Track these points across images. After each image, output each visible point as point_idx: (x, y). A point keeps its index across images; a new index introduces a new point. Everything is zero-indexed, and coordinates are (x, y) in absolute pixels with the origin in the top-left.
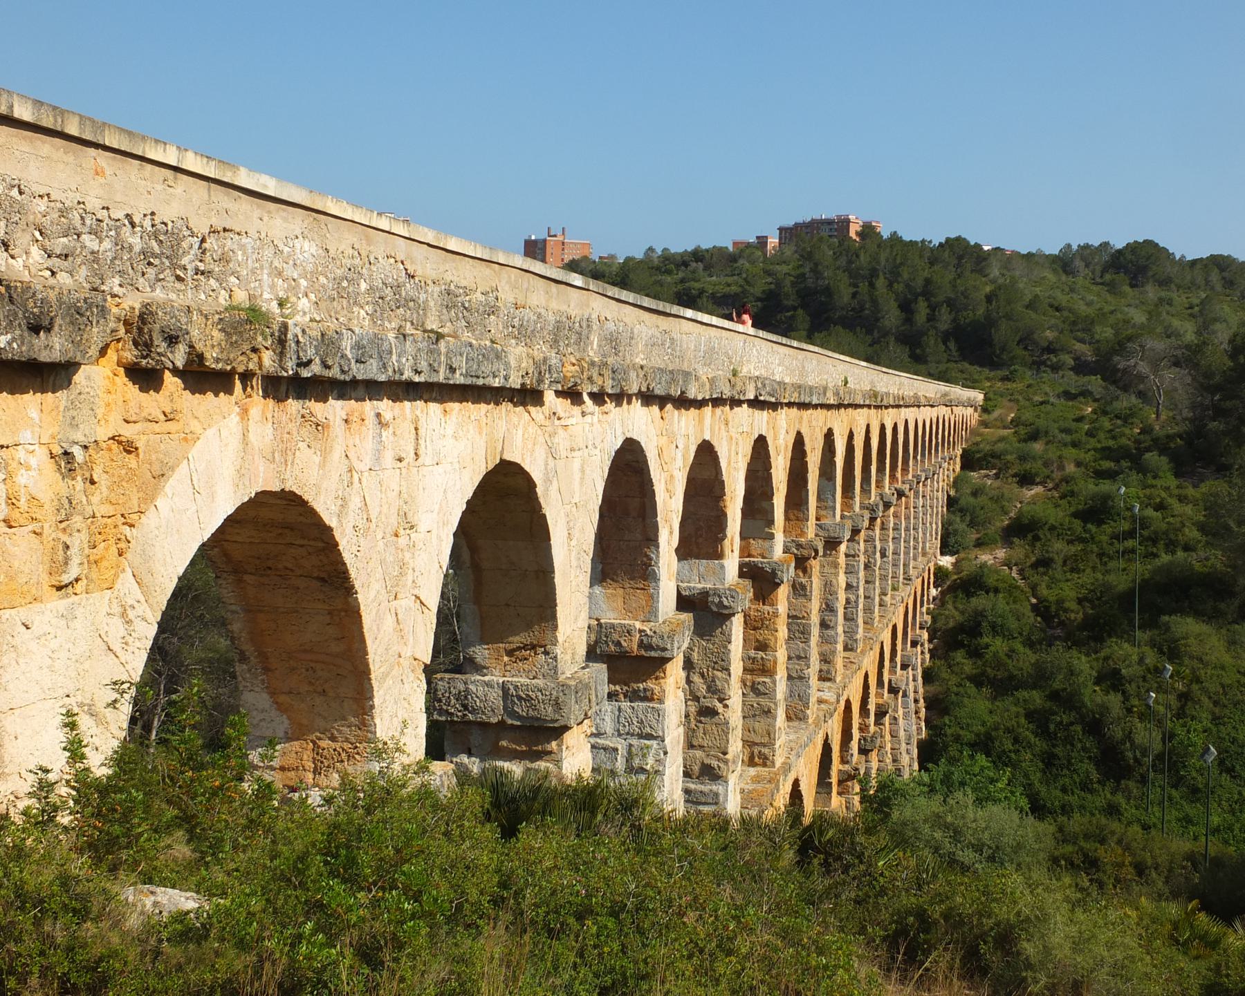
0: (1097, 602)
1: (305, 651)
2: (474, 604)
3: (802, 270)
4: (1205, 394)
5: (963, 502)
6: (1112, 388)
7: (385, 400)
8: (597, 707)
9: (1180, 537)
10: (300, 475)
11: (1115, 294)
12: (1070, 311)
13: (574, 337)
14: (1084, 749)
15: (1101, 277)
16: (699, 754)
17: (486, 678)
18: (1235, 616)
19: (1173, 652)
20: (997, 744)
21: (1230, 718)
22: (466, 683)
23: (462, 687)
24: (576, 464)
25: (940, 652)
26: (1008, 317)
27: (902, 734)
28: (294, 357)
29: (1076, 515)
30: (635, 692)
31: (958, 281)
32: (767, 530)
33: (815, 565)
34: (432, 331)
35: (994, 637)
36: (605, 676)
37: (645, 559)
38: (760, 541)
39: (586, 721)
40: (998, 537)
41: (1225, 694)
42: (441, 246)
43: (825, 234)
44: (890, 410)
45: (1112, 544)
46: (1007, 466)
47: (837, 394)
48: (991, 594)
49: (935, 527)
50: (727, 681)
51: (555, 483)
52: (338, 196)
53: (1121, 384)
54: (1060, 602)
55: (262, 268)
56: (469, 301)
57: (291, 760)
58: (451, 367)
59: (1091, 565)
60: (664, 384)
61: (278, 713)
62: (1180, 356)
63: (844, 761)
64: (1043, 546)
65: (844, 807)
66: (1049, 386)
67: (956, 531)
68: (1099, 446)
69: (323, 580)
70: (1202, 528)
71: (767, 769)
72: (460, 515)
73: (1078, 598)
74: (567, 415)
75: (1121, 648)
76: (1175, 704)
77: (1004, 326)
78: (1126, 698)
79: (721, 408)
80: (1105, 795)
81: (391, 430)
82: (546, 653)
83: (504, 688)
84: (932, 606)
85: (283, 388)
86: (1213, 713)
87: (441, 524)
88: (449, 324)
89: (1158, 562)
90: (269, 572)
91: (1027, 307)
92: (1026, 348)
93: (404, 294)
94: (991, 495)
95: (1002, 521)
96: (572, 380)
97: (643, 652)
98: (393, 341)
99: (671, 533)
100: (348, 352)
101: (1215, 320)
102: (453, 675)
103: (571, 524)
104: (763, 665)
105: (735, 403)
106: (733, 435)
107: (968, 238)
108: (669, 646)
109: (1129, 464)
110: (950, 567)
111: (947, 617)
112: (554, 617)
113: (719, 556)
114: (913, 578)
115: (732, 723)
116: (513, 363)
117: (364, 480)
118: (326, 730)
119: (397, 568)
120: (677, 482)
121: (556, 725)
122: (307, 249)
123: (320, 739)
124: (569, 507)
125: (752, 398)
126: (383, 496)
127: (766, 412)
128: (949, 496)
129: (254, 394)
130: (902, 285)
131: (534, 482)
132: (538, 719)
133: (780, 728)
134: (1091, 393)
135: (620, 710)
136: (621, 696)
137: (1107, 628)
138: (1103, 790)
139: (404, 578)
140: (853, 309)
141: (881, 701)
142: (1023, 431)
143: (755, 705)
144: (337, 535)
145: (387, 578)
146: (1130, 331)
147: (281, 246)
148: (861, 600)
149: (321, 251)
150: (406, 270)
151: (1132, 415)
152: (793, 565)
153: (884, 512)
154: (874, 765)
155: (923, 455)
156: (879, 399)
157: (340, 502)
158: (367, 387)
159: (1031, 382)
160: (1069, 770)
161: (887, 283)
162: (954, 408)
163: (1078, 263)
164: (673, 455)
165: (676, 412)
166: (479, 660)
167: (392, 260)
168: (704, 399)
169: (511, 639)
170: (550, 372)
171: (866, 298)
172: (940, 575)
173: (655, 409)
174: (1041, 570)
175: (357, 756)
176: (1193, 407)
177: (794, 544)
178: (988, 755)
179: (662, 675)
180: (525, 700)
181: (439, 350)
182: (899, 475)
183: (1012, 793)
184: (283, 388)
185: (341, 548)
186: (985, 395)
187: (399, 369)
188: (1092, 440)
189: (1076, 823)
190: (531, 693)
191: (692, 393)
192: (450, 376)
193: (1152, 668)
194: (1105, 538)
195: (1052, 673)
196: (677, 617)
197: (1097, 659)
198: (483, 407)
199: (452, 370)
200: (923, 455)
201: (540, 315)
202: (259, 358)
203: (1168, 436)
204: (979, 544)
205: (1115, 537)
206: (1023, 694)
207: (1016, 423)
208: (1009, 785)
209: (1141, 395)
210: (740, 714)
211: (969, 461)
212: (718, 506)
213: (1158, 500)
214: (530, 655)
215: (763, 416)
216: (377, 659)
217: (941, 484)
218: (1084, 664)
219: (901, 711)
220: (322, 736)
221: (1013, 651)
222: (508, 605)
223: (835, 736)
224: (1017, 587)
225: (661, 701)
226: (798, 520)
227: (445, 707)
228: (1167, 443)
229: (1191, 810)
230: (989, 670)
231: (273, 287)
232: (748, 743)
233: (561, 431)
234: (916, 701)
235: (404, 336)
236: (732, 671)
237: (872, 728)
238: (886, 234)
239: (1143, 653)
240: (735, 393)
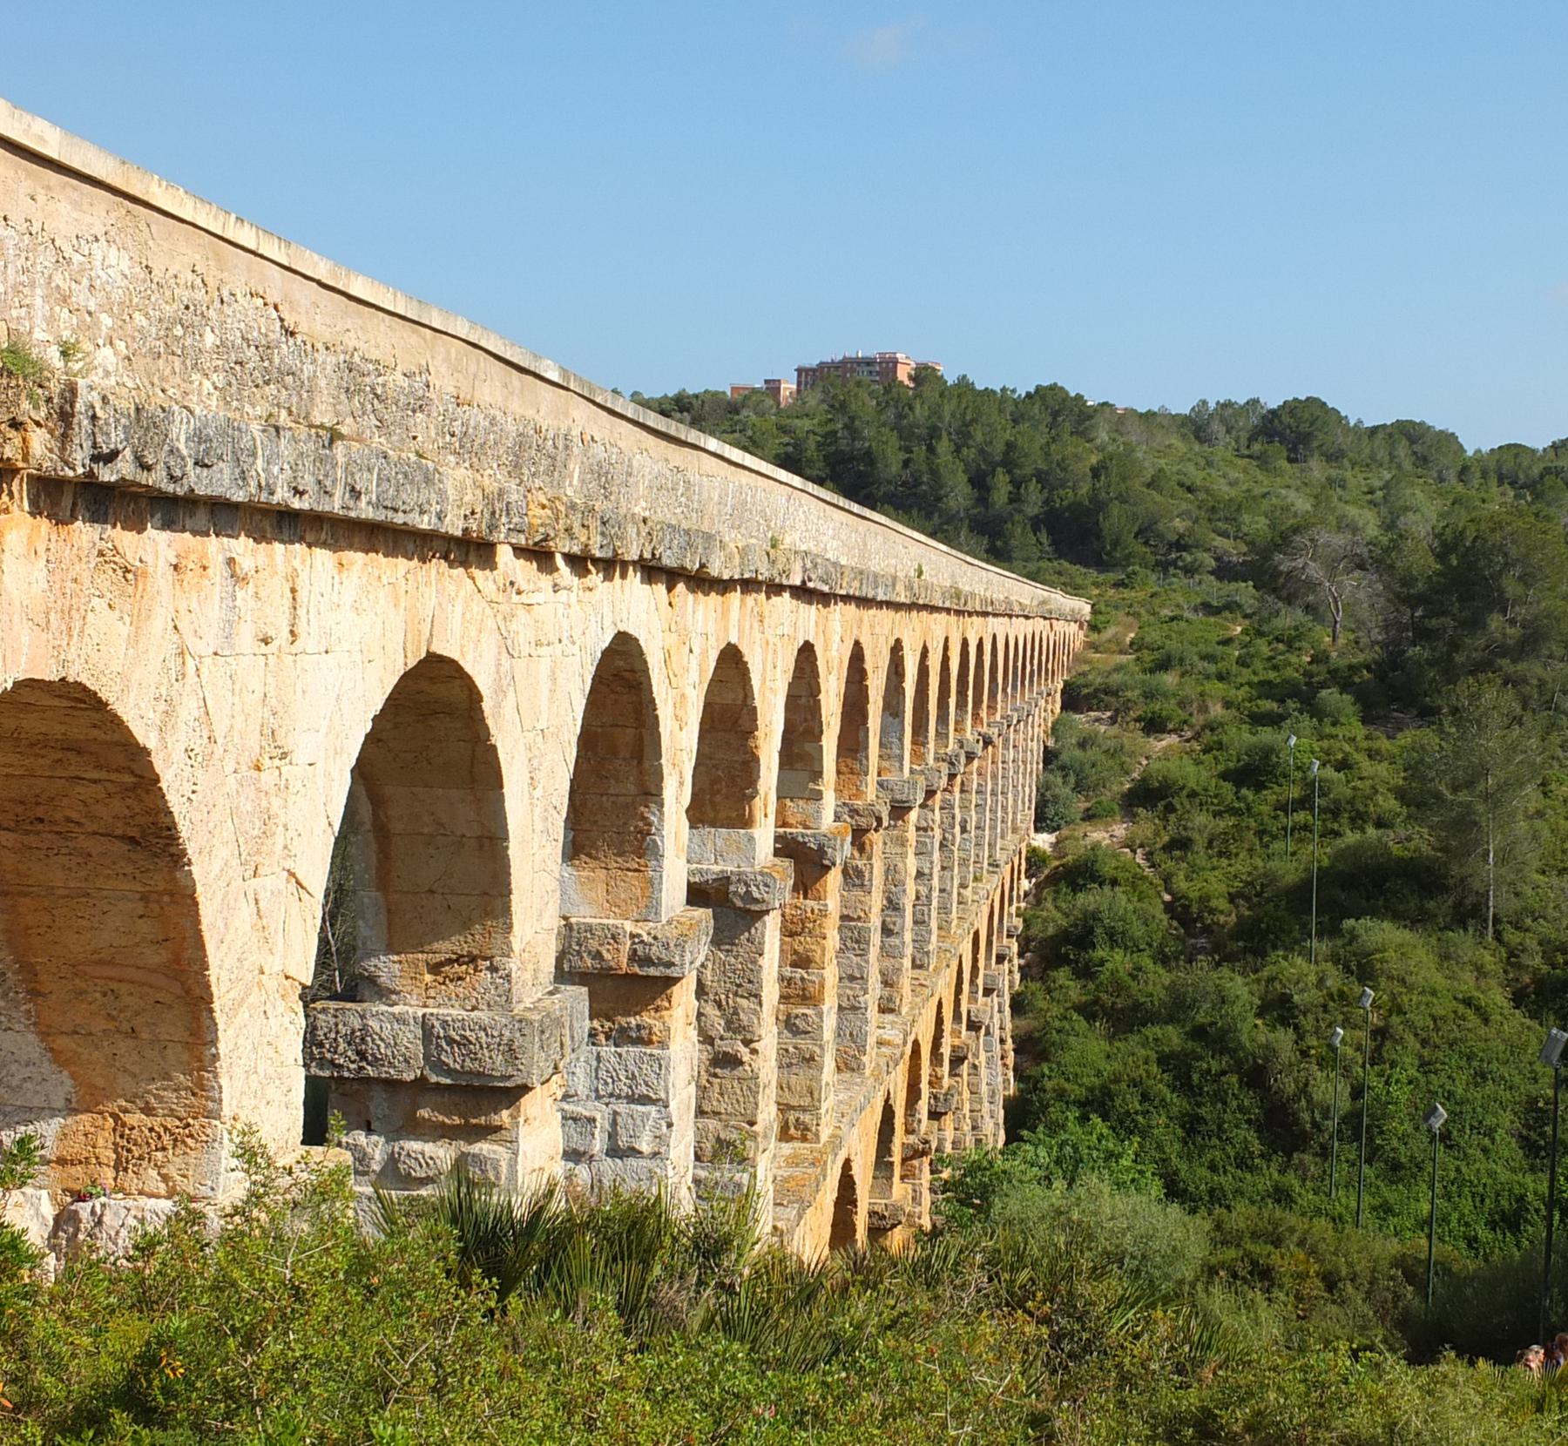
0: (1255, 900)
1: (101, 962)
2: (378, 889)
3: (830, 427)
4: (1402, 608)
5: (1064, 758)
6: (1270, 599)
7: (243, 538)
8: (573, 1056)
9: (1372, 809)
10: (95, 656)
11: (1267, 470)
12: (1207, 491)
13: (545, 462)
14: (1241, 1109)
15: (1248, 447)
16: (712, 1124)
17: (396, 1009)
18: (1448, 919)
19: (1363, 969)
20: (1118, 1102)
21: (1444, 1063)
22: (363, 1017)
23: (357, 1023)
24: (544, 667)
25: (1035, 970)
26: (1122, 499)
27: (984, 1089)
28: (87, 444)
29: (1225, 776)
30: (623, 1031)
31: (1053, 447)
32: (811, 785)
33: (876, 839)
34: (322, 426)
35: (1112, 948)
36: (584, 1006)
37: (641, 824)
38: (801, 803)
39: (554, 1077)
40: (1116, 807)
41: (1437, 1029)
42: (340, 287)
43: (865, 378)
44: (974, 618)
45: (1275, 818)
46: (1127, 706)
47: (909, 587)
48: (1107, 888)
49: (1029, 791)
50: (756, 1013)
51: (511, 694)
52: (172, 179)
53: (1284, 593)
54: (1204, 899)
55: (32, 285)
56: (384, 385)
57: (76, 1148)
58: (353, 490)
59: (1247, 846)
60: (676, 549)
61: (54, 1067)
62: (1366, 555)
63: (909, 1131)
64: (1180, 820)
65: (910, 1197)
66: (1181, 594)
67: (1055, 797)
68: (1255, 679)
69: (132, 840)
70: (1401, 795)
71: (807, 1145)
72: (362, 739)
73: (1229, 894)
74: (532, 587)
75: (1292, 965)
76: (1369, 1044)
77: (1116, 510)
78: (1301, 1037)
79: (754, 595)
80: (1270, 1175)
81: (251, 588)
82: (493, 969)
83: (425, 1025)
84: (1023, 905)
85: (67, 502)
86: (1421, 1057)
87: (331, 753)
88: (349, 420)
89: (1340, 843)
90: (40, 827)
91: (1149, 485)
92: (1146, 543)
93: (277, 360)
94: (1104, 748)
95: (1122, 784)
96: (542, 530)
97: (636, 969)
98: (257, 434)
99: (681, 784)
100: (182, 446)
101: (1406, 509)
102: (341, 1004)
103: (535, 763)
104: (804, 989)
105: (774, 589)
106: (772, 640)
107: (1067, 388)
108: (677, 960)
109: (1299, 705)
110: (1049, 850)
111: (1045, 920)
112: (507, 911)
113: (746, 822)
114: (1002, 863)
115: (763, 1079)
116: (452, 493)
117: (204, 670)
118: (136, 1096)
119: (258, 824)
120: (690, 704)
121: (508, 1084)
122: (114, 263)
123: (126, 1111)
124: (531, 735)
125: (798, 582)
126: (236, 700)
127: (814, 607)
128: (1046, 747)
129: (14, 508)
130: (973, 450)
131: (479, 693)
132: (479, 1074)
133: (827, 1084)
134: (1239, 606)
135: (598, 1058)
136: (602, 1037)
137: (1272, 937)
138: (1268, 1168)
139: (270, 841)
140: (904, 484)
141: (957, 1042)
142: (1147, 656)
143: (791, 1049)
144: (158, 764)
145: (241, 840)
146: (1291, 521)
147: (68, 252)
148: (935, 894)
149: (138, 269)
150: (282, 320)
151: (1299, 637)
152: (849, 839)
153: (966, 766)
154: (949, 1135)
155: (1014, 687)
156: (963, 601)
157: (162, 706)
158: (212, 512)
159: (1156, 589)
160: (1220, 1138)
161: (952, 448)
162: (1054, 622)
163: (1217, 427)
164: (685, 662)
165: (691, 596)
166: (384, 979)
167: (260, 302)
168: (731, 580)
169: (436, 946)
170: (508, 514)
171: (924, 468)
172: (1035, 860)
173: (661, 588)
174: (1177, 853)
175: (189, 1141)
176: (1386, 628)
177: (846, 809)
178: (1105, 1118)
179: (667, 1005)
180: (459, 1044)
181: (334, 458)
182: (984, 714)
183: (1141, 1172)
184: (67, 502)
185: (163, 785)
186: (1093, 606)
187: (268, 485)
188: (1244, 671)
189: (1241, 1216)
190: (468, 1033)
191: (715, 569)
192: (351, 504)
193: (1335, 993)
194: (1265, 809)
195: (1195, 1000)
196: (689, 914)
197: (1258, 981)
198: (401, 562)
199: (355, 494)
200: (1014, 687)
201: (493, 421)
202: (24, 440)
203: (1351, 667)
204: (1089, 816)
205: (1282, 807)
206: (1153, 1031)
207: (1137, 646)
208: (1135, 1161)
209: (1309, 609)
210: (774, 1063)
211: (1073, 699)
212: (745, 746)
213: (1340, 756)
214: (467, 973)
215: (810, 613)
216: (224, 975)
217: (1036, 729)
218: (1240, 988)
219: (983, 1056)
220: (129, 1105)
221: (1140, 969)
222: (431, 892)
223: (899, 1093)
224: (1144, 878)
225: (663, 1045)
226: (852, 773)
227: (328, 1056)
228: (1350, 677)
229: (1391, 1195)
230: (1104, 996)
231: (51, 320)
232: (784, 1108)
233: (521, 612)
234: (1002, 1041)
235: (277, 429)
236: (763, 998)
237: (946, 1082)
238: (951, 380)
239: (1323, 971)
240: (775, 573)
